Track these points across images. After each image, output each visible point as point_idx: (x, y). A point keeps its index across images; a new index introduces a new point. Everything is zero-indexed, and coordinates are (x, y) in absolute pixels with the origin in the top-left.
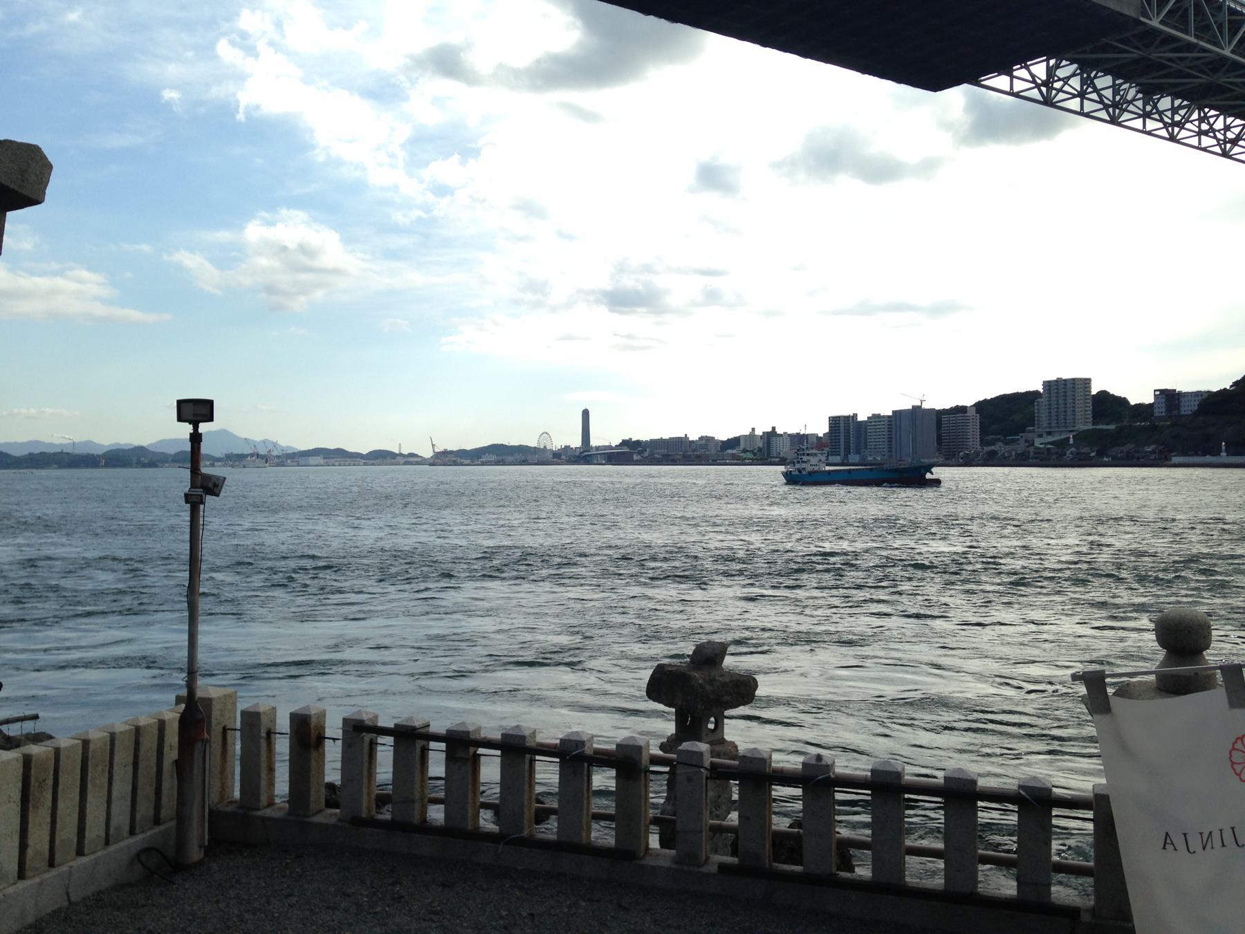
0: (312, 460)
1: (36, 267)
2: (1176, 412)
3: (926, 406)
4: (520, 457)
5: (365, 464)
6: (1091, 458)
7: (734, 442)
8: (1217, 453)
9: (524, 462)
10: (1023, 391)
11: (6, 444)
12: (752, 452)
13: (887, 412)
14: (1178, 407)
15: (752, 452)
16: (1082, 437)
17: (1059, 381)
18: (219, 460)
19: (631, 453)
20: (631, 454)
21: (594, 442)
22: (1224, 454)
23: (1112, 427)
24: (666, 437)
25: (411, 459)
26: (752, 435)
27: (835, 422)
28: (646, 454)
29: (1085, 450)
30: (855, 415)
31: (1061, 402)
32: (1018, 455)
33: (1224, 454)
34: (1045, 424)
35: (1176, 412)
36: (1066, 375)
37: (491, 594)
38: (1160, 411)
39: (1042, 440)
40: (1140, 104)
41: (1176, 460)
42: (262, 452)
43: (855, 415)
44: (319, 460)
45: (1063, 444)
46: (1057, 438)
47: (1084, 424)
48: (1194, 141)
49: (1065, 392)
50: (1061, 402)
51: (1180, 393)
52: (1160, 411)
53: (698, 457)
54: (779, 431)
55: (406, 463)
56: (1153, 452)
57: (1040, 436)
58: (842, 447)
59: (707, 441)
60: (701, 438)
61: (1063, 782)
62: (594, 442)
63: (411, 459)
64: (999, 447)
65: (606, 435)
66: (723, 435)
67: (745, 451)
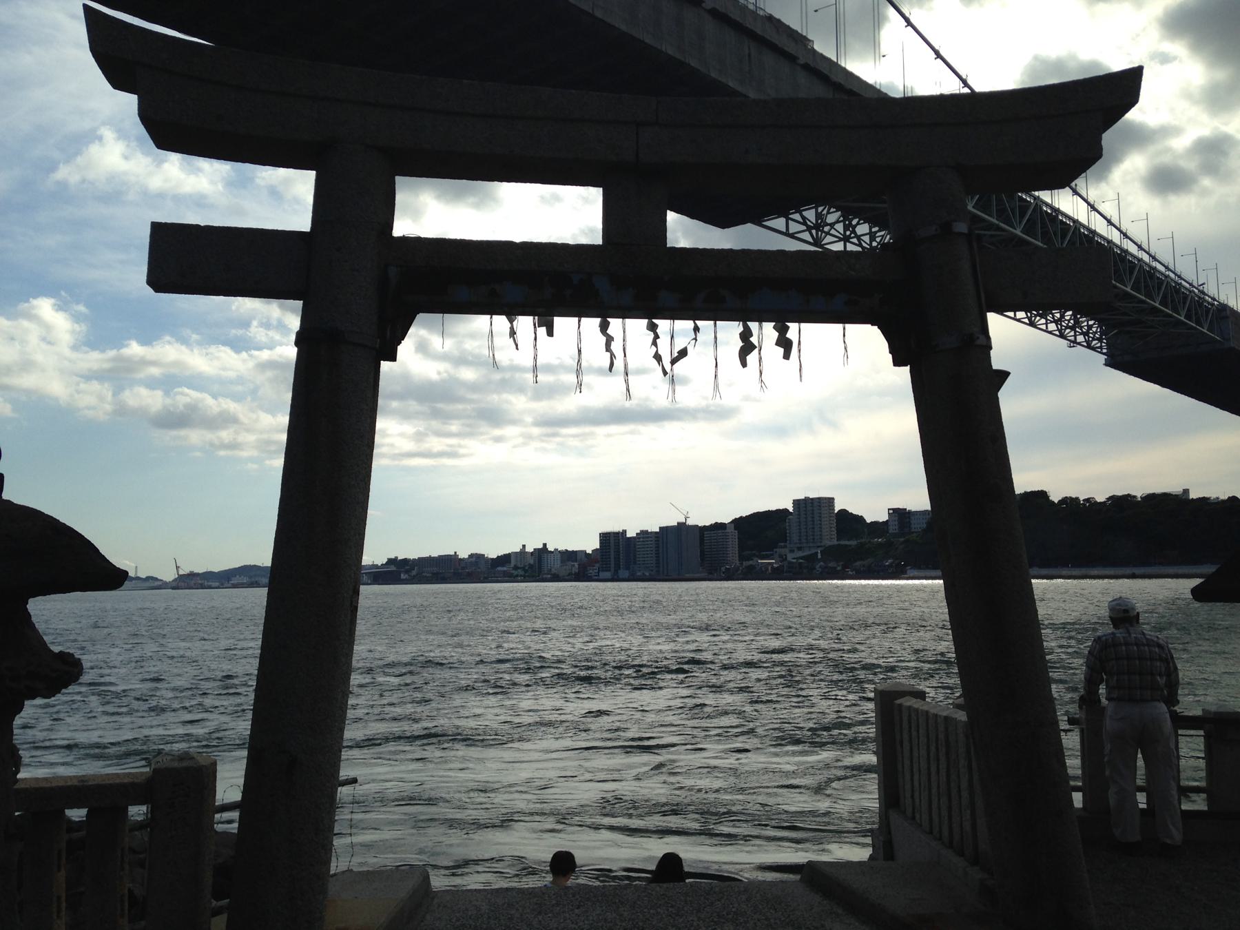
3: (690, 522)
7: (504, 559)
12: (523, 569)
15: (523, 569)
17: (807, 499)
23: (853, 543)
27: (605, 538)
29: (831, 564)
34: (795, 538)
38: (893, 529)
40: (840, 227)
43: (625, 532)
45: (811, 558)
47: (830, 538)
48: (1044, 327)
51: (910, 512)
53: (469, 574)
54: (551, 548)
57: (792, 551)
59: (477, 558)
60: (471, 556)
66: (492, 554)
67: (516, 568)
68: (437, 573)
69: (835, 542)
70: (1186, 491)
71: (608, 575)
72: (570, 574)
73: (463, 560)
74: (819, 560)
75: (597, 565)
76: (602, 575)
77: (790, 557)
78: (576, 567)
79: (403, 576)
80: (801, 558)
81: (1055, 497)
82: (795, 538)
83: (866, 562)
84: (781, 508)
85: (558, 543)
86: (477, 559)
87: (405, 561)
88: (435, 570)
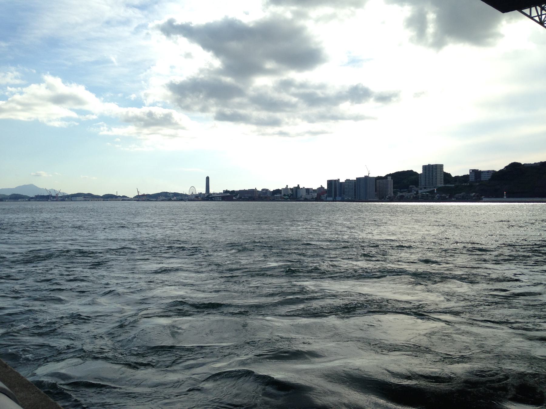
0: (78, 198)
1: (40, 101)
2: (478, 180)
3: (371, 176)
4: (180, 197)
5: (103, 200)
6: (447, 199)
7: (277, 191)
8: (502, 197)
9: (182, 200)
10: (406, 170)
11: (2, 189)
12: (288, 195)
13: (353, 178)
14: (480, 177)
15: (288, 195)
16: (439, 189)
17: (429, 165)
18: (32, 198)
19: (229, 196)
20: (232, 197)
21: (211, 191)
23: (453, 185)
24: (247, 189)
25: (125, 198)
26: (286, 189)
27: (330, 183)
28: (238, 196)
29: (443, 195)
30: (339, 180)
31: (431, 174)
32: (413, 197)
34: (423, 183)
35: (478, 180)
36: (432, 163)
37: (342, 263)
38: (472, 179)
39: (422, 191)
41: (484, 199)
42: (54, 194)
43: (339, 180)
44: (82, 198)
45: (432, 192)
46: (428, 190)
47: (440, 184)
49: (432, 170)
50: (431, 174)
51: (480, 171)
52: (472, 179)
53: (266, 198)
54: (301, 187)
55: (123, 200)
56: (474, 196)
57: (421, 189)
58: (333, 193)
59: (265, 191)
60: (263, 190)
61: (85, 310)
62: (211, 191)
63: (124, 198)
64: (405, 194)
65: (216, 189)
66: (271, 189)
67: (285, 195)
68: (251, 197)
69: (443, 185)
71: (331, 199)
72: (312, 198)
73: (258, 191)
74: (436, 193)
75: (325, 195)
76: (328, 199)
77: (420, 191)
78: (319, 195)
79: (234, 198)
80: (427, 192)
82: (423, 183)
83: (462, 194)
84: (410, 169)
85: (305, 184)
86: (265, 191)
87: (233, 192)
88: (250, 195)
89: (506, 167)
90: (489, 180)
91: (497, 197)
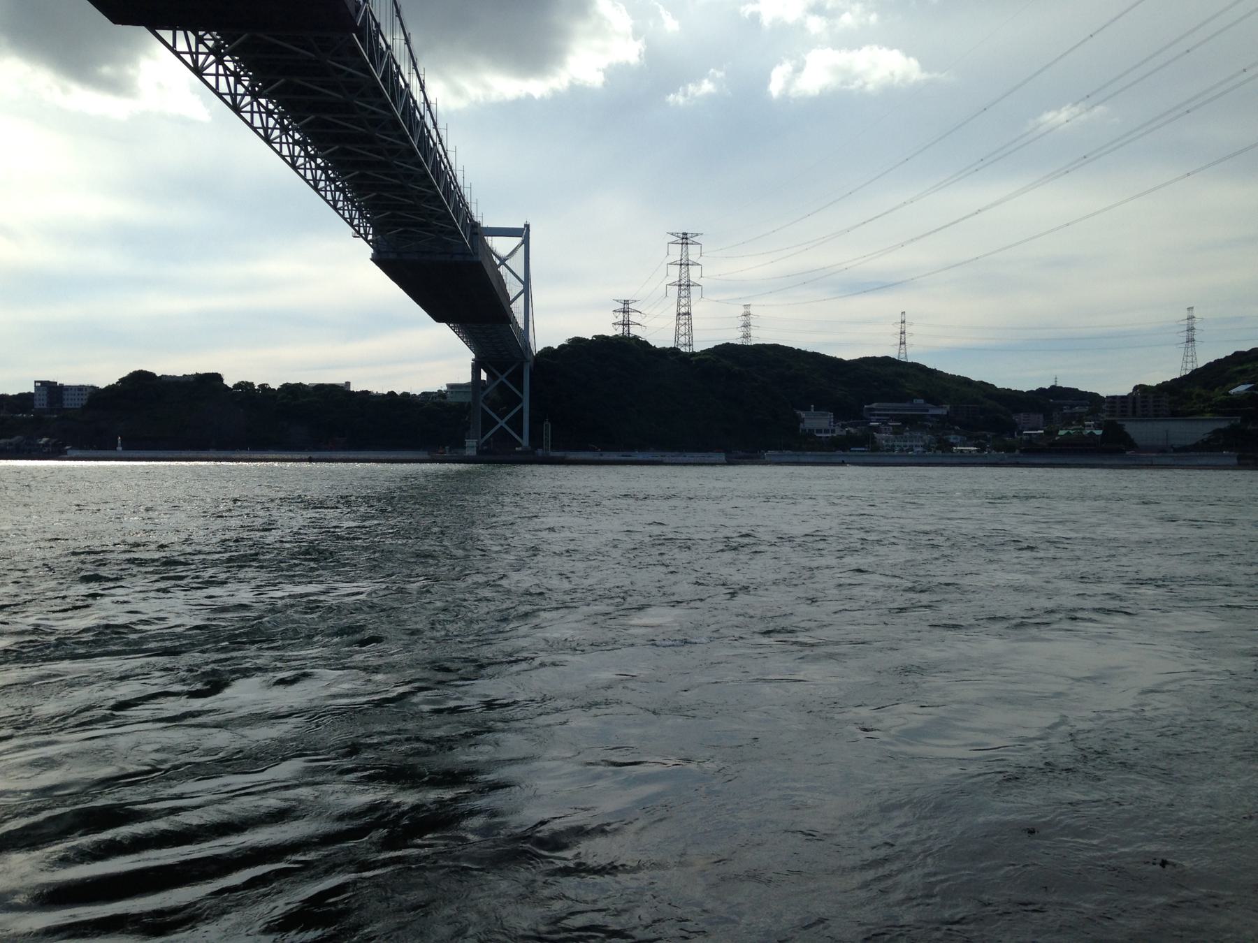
22: (120, 448)
33: (120, 448)
51: (62, 386)
70: (348, 384)
81: (230, 381)
89: (122, 380)
90: (83, 407)
91: (101, 447)
